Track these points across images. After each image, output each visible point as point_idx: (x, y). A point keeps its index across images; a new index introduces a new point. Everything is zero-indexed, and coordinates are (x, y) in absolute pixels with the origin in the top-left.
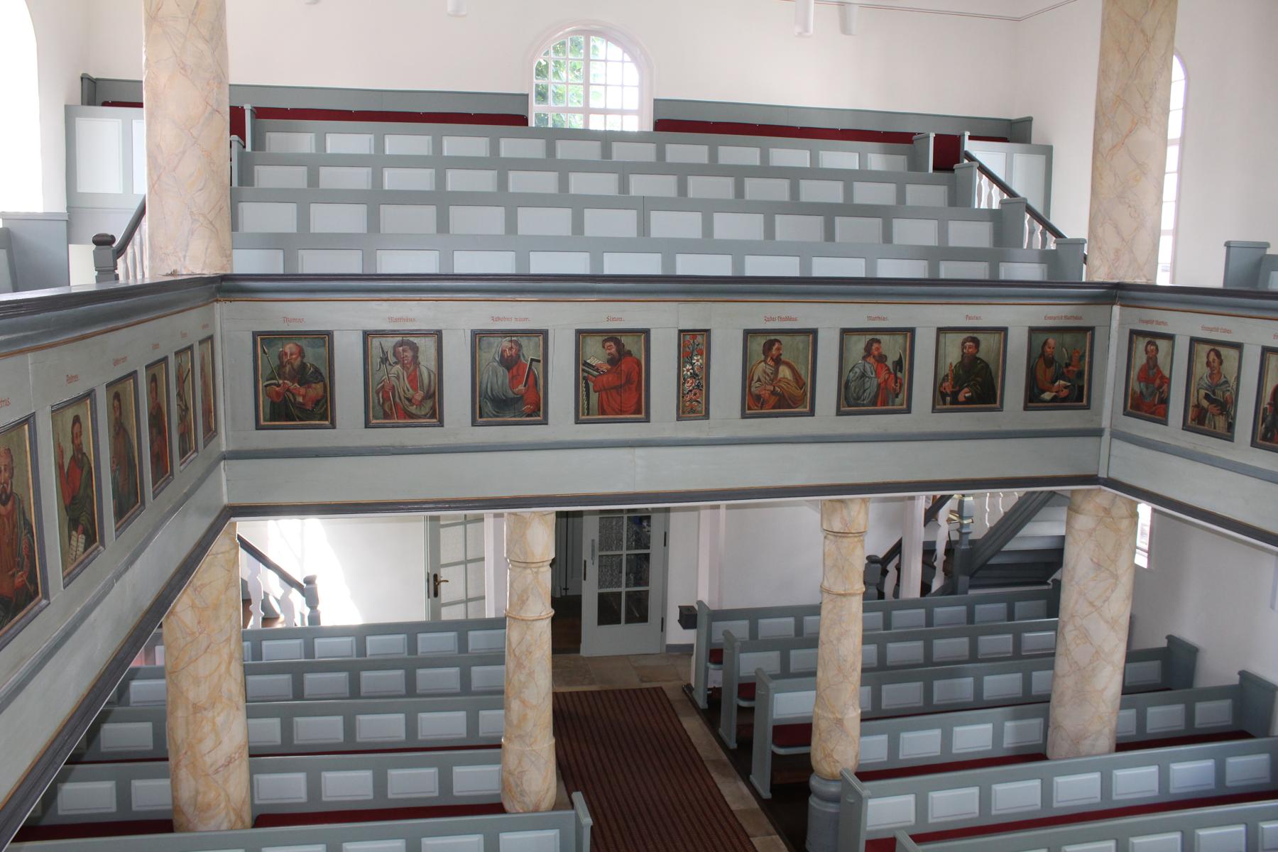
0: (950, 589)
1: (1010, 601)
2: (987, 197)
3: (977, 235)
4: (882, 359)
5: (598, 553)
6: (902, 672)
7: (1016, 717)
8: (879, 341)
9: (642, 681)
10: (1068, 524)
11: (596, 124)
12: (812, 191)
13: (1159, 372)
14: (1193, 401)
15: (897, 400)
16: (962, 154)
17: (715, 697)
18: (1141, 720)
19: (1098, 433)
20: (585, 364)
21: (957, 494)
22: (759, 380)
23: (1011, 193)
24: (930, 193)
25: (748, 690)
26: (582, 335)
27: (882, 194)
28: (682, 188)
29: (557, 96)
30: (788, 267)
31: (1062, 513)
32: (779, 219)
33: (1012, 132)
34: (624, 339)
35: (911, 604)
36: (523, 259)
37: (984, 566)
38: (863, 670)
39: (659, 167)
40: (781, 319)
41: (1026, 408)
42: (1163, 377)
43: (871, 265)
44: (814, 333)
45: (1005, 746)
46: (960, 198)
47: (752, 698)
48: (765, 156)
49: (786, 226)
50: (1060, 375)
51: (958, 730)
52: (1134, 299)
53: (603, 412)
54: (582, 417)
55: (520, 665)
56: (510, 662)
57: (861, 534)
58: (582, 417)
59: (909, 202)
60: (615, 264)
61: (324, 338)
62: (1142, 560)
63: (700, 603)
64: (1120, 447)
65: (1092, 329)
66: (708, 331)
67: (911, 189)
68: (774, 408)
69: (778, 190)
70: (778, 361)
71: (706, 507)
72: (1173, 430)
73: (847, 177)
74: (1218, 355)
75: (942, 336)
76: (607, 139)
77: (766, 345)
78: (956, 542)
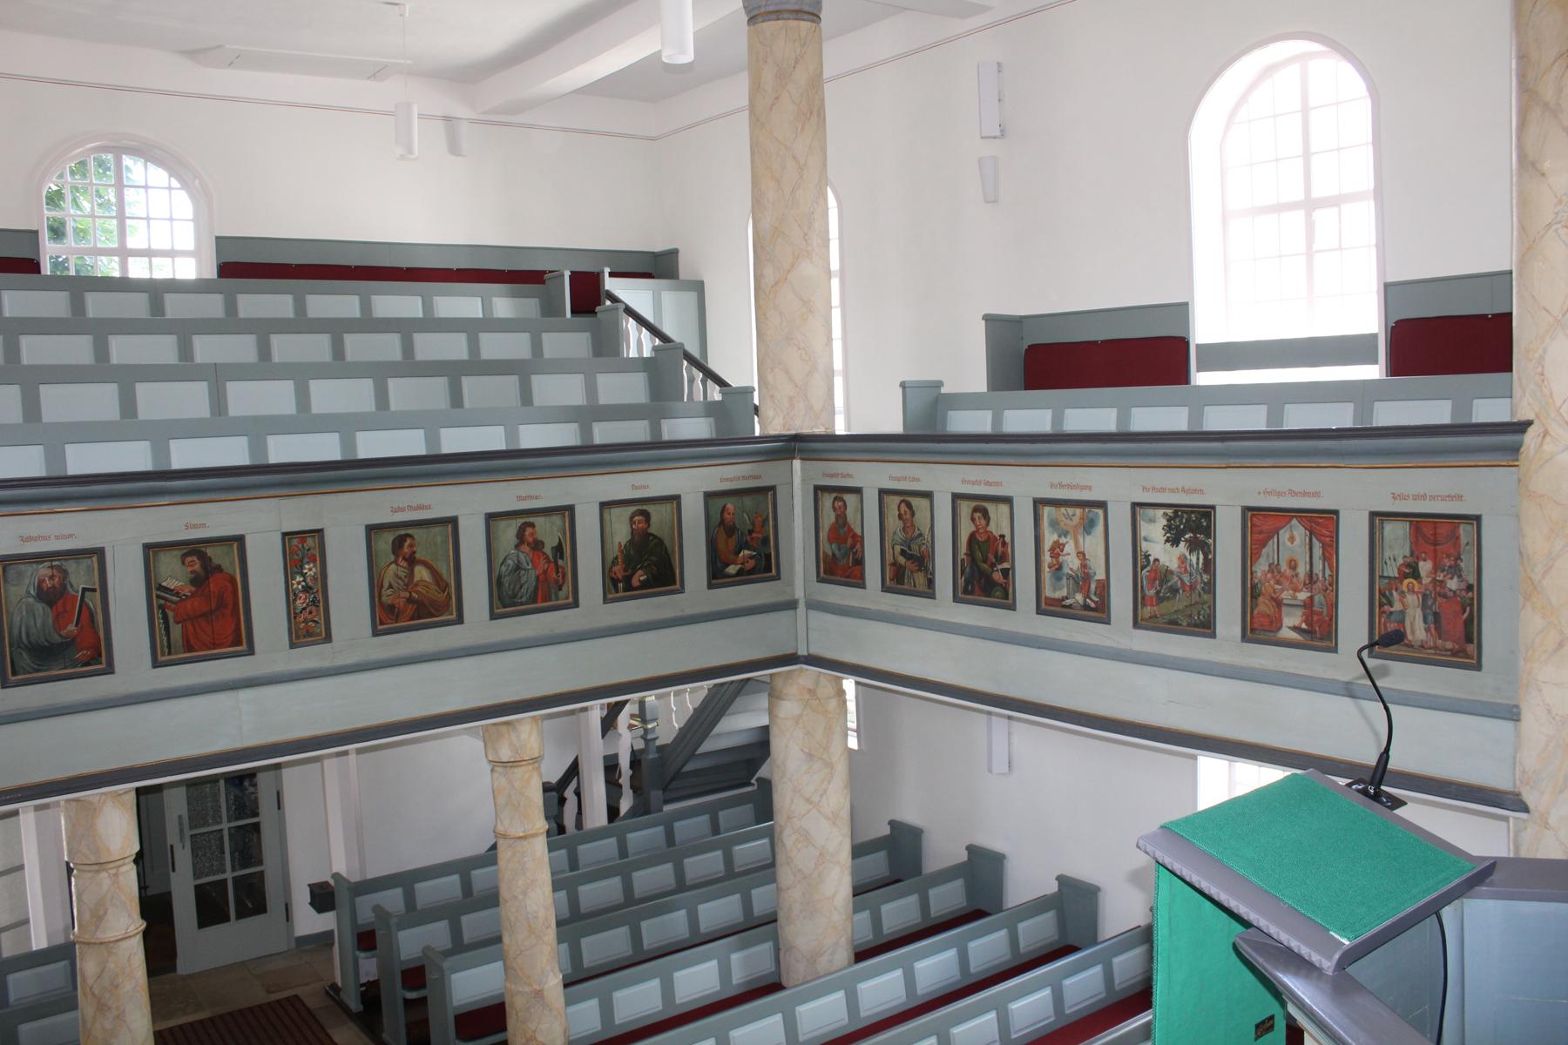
0: (642, 808)
1: (713, 811)
2: (639, 344)
3: (627, 389)
4: (537, 545)
5: (188, 833)
6: (602, 918)
7: (743, 946)
8: (532, 525)
9: (269, 992)
10: (771, 712)
11: (138, 270)
12: (430, 347)
13: (850, 530)
14: (889, 559)
15: (562, 594)
16: (603, 295)
17: (371, 994)
18: (877, 921)
19: (791, 605)
21: (636, 696)
22: (391, 586)
23: (664, 338)
24: (569, 342)
25: (415, 976)
26: (152, 550)
27: (514, 346)
28: (264, 351)
29: (81, 233)
30: (410, 443)
31: (763, 701)
32: (393, 384)
33: (657, 266)
34: (210, 551)
35: (598, 834)
36: (55, 455)
37: (678, 775)
38: (559, 924)
39: (230, 324)
40: (411, 508)
41: (710, 586)
42: (855, 536)
43: (512, 434)
44: (453, 522)
45: (735, 982)
46: (607, 346)
47: (423, 985)
48: (366, 306)
49: (403, 392)
50: (744, 545)
51: (679, 975)
52: (814, 451)
54: (161, 659)
55: (102, 1007)
56: (86, 1007)
57: (535, 760)
58: (161, 659)
59: (548, 353)
60: (185, 455)
62: (853, 743)
63: (336, 876)
64: (818, 618)
65: (773, 488)
66: (320, 532)
67: (548, 338)
68: (412, 619)
69: (387, 347)
70: (412, 561)
71: (330, 756)
72: (872, 594)
73: (470, 328)
74: (909, 505)
75: (606, 512)
76: (156, 291)
77: (395, 543)
78: (642, 751)
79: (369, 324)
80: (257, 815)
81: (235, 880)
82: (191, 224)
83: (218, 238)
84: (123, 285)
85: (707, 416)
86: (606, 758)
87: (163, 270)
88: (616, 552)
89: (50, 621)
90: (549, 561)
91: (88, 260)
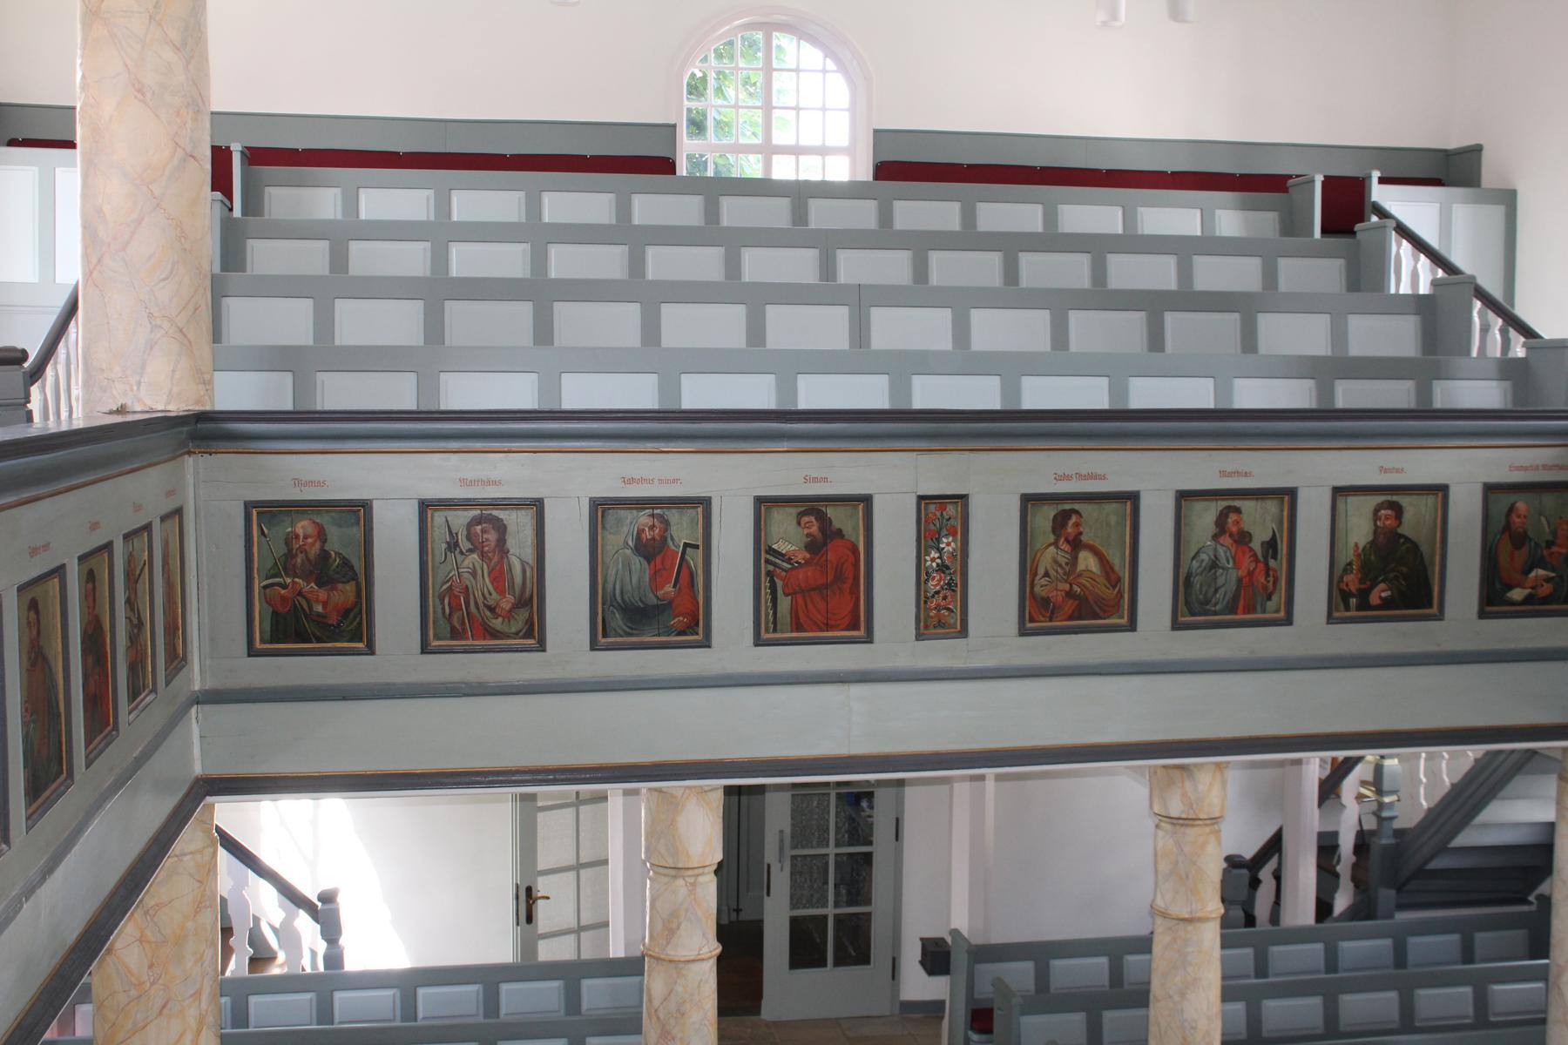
0: (1363, 910)
1: (1467, 931)
2: (1411, 274)
3: (1394, 337)
4: (1243, 538)
5: (789, 852)
8: (1238, 511)
11: (783, 170)
12: (1127, 272)
15: (1270, 605)
16: (1368, 209)
20: (770, 551)
21: (1371, 755)
22: (1047, 574)
23: (1450, 268)
24: (1320, 271)
26: (764, 505)
27: (1240, 274)
30: (1090, 394)
33: (1449, 169)
34: (831, 512)
39: (884, 237)
40: (1080, 476)
41: (1482, 615)
43: (1223, 389)
44: (1133, 498)
46: (1366, 278)
48: (1050, 218)
49: (1086, 329)
53: (798, 627)
54: (765, 636)
58: (765, 636)
60: (815, 393)
61: (358, 512)
63: (955, 933)
66: (962, 499)
68: (1070, 618)
69: (1073, 270)
70: (1076, 544)
71: (962, 779)
73: (1182, 248)
75: (1340, 501)
76: (801, 194)
77: (1056, 518)
78: (1372, 833)
79: (1052, 241)
80: (870, 843)
81: (839, 919)
82: (846, 115)
83: (876, 131)
84: (764, 188)
85: (1502, 378)
86: (1321, 835)
87: (810, 170)
88: (1351, 556)
89: (647, 579)
90: (1257, 561)
91: (731, 158)
